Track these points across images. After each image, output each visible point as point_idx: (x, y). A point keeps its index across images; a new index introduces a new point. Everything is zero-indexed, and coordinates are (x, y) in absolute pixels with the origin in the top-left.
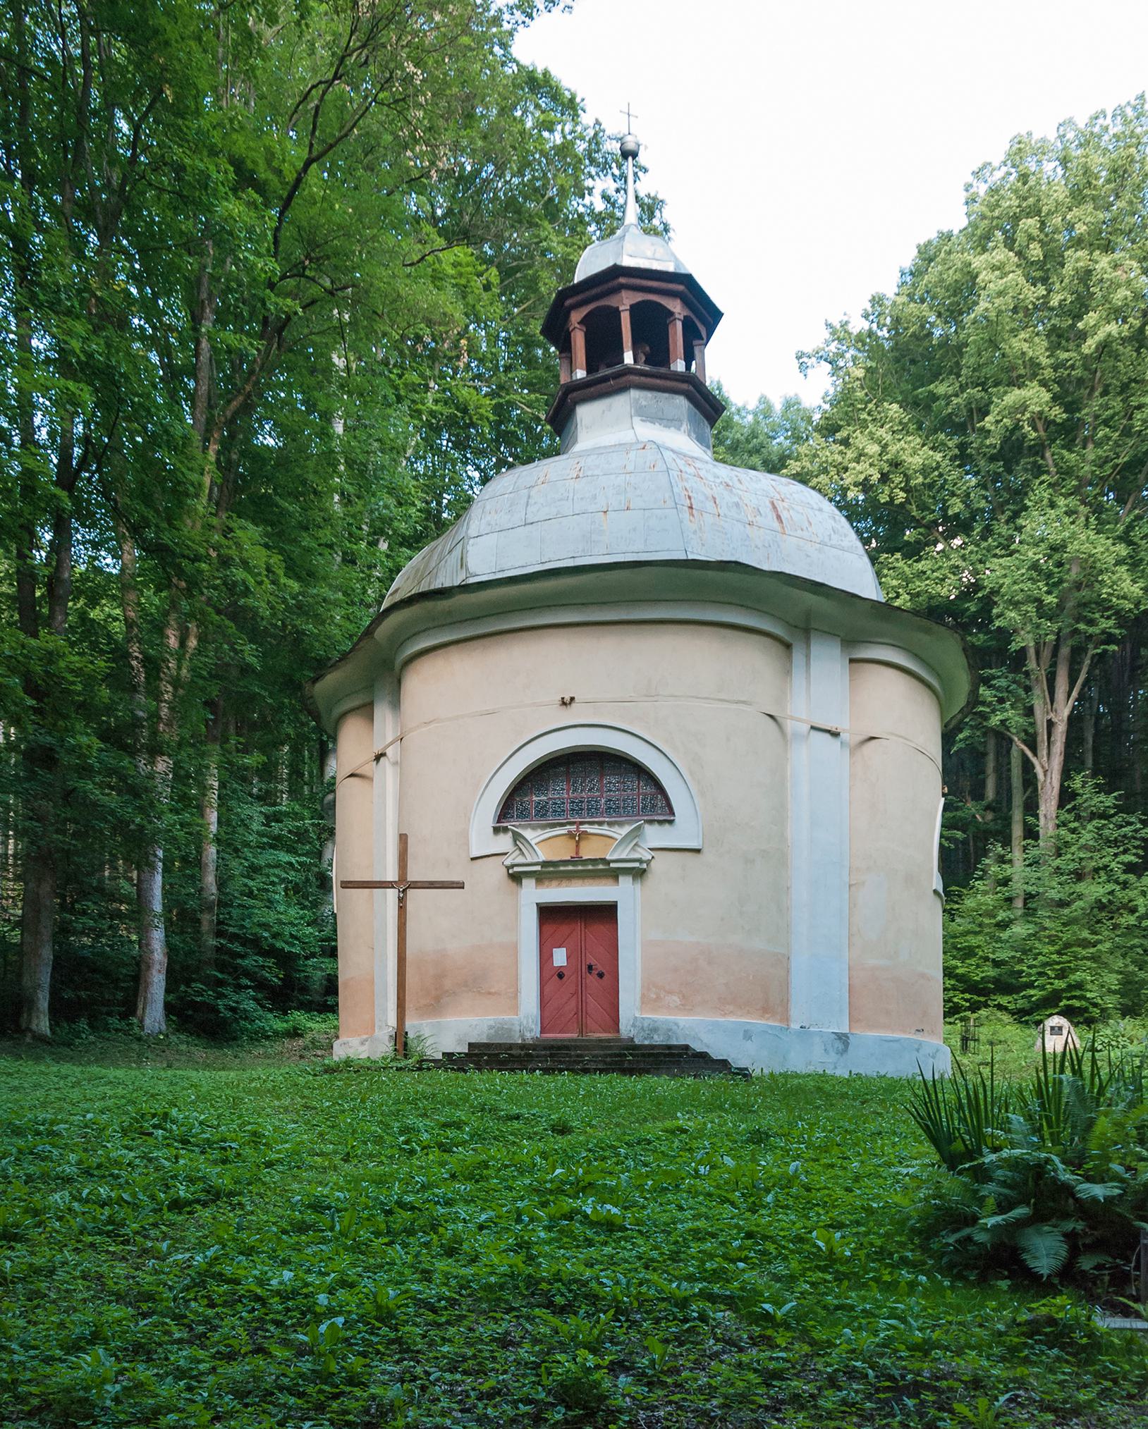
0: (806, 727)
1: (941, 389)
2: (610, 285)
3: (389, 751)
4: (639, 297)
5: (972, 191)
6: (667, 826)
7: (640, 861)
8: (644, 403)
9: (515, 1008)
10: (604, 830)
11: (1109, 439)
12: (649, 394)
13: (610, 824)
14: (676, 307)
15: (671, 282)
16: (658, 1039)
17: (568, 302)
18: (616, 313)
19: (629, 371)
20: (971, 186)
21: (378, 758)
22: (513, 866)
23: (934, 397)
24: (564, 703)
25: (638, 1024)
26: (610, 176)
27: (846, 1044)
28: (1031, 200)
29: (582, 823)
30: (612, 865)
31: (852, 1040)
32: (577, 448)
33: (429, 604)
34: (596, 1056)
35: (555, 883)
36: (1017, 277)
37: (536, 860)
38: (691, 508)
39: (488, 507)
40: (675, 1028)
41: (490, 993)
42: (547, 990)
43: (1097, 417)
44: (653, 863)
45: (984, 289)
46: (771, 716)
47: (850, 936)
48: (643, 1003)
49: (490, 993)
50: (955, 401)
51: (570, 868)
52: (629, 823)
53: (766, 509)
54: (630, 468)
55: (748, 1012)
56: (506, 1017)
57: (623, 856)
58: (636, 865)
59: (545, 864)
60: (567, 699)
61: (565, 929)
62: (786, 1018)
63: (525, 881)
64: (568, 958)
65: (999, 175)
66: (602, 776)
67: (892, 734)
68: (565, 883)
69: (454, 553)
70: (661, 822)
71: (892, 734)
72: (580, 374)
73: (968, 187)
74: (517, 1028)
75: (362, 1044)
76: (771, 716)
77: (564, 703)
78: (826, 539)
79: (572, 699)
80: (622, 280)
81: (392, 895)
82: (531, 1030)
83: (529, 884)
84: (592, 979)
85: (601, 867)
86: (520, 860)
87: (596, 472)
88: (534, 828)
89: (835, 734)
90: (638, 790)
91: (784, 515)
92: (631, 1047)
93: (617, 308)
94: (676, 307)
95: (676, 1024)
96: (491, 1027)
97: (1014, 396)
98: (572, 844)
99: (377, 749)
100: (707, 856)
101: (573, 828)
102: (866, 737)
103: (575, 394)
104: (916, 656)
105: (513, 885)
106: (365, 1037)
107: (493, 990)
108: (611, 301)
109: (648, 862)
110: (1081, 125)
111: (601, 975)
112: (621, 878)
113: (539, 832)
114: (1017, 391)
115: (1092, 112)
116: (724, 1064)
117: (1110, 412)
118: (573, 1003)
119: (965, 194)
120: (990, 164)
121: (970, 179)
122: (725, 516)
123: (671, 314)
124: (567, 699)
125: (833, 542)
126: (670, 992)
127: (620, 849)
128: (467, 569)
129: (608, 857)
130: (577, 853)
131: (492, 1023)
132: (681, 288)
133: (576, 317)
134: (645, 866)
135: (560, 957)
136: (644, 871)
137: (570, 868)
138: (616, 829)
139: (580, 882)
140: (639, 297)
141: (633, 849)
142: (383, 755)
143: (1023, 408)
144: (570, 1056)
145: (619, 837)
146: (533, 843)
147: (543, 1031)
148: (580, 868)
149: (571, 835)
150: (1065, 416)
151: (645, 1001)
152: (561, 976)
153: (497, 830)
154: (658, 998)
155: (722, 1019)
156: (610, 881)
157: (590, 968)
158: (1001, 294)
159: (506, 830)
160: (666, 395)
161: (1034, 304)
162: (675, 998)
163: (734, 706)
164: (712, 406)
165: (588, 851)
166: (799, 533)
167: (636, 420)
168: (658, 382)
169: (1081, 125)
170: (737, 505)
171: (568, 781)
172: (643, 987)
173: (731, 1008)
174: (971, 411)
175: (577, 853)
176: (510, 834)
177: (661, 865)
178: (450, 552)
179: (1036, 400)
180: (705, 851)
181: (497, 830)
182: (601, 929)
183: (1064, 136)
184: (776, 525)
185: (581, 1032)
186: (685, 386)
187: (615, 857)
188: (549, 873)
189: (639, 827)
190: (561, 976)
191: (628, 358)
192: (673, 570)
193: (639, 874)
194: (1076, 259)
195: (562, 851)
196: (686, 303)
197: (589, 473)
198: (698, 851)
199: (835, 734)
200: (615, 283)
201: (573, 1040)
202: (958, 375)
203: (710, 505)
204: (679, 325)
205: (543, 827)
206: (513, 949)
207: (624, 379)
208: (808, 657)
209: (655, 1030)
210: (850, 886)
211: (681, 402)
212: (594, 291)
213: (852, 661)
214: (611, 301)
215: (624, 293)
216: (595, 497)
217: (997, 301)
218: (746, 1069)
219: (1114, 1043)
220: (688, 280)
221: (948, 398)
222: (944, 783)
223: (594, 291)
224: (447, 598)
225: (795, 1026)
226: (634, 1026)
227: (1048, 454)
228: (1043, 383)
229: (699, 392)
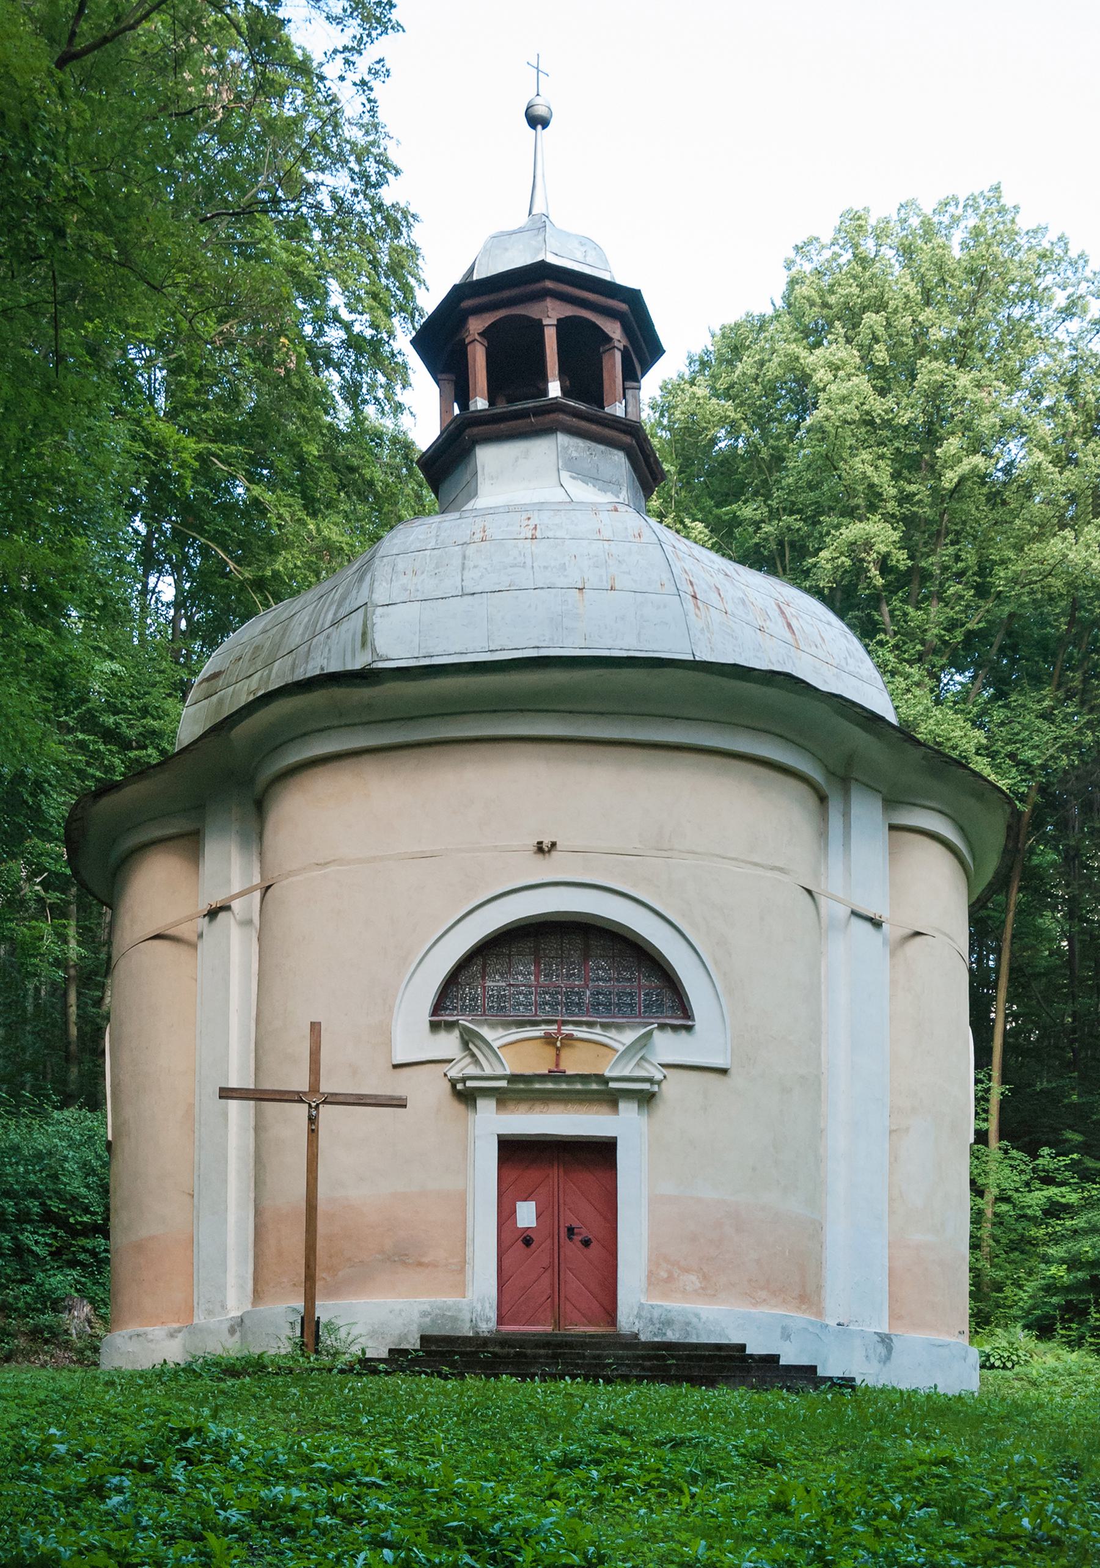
0: (843, 912)
1: (747, 511)
2: (538, 286)
3: (236, 905)
4: (569, 311)
5: (794, 270)
6: (683, 1034)
7: (650, 1080)
8: (574, 454)
9: (460, 1288)
10: (596, 1034)
11: (961, 597)
12: (580, 443)
13: (605, 1026)
14: (614, 330)
15: (612, 297)
16: (672, 1336)
17: (467, 304)
18: (538, 327)
19: (555, 407)
20: (793, 262)
21: (213, 914)
22: (464, 1080)
23: (736, 521)
24: (540, 849)
25: (644, 1313)
26: (346, 172)
27: (890, 1349)
28: (874, 291)
30: (612, 1085)
31: (896, 1343)
32: (482, 501)
33: (339, 693)
34: (622, 1358)
35: (523, 1107)
36: (862, 383)
37: (499, 1072)
38: (694, 597)
39: (400, 566)
40: (694, 1320)
43: (945, 568)
44: (664, 1085)
45: (824, 389)
46: (809, 892)
47: (891, 1200)
48: (649, 1284)
49: (420, 1264)
50: (766, 528)
51: (550, 1086)
52: (632, 1026)
53: (774, 613)
54: (607, 534)
55: (784, 1301)
56: (450, 1300)
57: (626, 1073)
58: (646, 1086)
59: (513, 1078)
60: (547, 842)
61: (533, 1175)
62: (820, 1313)
63: (481, 1103)
65: (827, 254)
66: (586, 957)
67: (938, 930)
68: (538, 1107)
69: (345, 626)
70: (675, 1028)
71: (938, 930)
72: (480, 403)
73: (789, 265)
74: (467, 1317)
75: (172, 1335)
76: (809, 892)
77: (540, 849)
78: (843, 663)
79: (554, 844)
80: (549, 284)
81: (300, 1111)
82: (488, 1320)
83: (486, 1107)
84: (572, 1249)
85: (594, 1086)
86: (472, 1070)
87: (559, 534)
88: (493, 1026)
89: (876, 924)
90: (645, 984)
91: (794, 623)
92: (631, 1343)
93: (540, 321)
94: (614, 330)
95: (697, 1316)
96: (425, 1314)
97: (853, 531)
99: (216, 900)
100: (736, 1079)
101: (553, 1028)
102: (909, 931)
103: (475, 430)
104: (962, 829)
105: (459, 1108)
106: (176, 1326)
107: (425, 1260)
108: (532, 311)
109: (659, 1083)
110: (928, 210)
111: (586, 1243)
112: (622, 1105)
113: (501, 1032)
114: (859, 525)
115: (942, 197)
116: (807, 1373)
117: (961, 565)
118: (546, 1280)
119: (785, 273)
120: (817, 239)
121: (792, 254)
122: (733, 615)
123: (608, 339)
124: (547, 842)
125: (851, 668)
126: (687, 1270)
127: (624, 1062)
128: (374, 650)
130: (557, 1065)
131: (427, 1307)
132: (624, 307)
133: (476, 326)
134: (656, 1088)
135: (526, 1215)
136: (653, 1095)
137: (550, 1086)
138: (613, 1033)
139: (561, 1107)
140: (569, 311)
141: (638, 1064)
142: (226, 908)
143: (868, 546)
144: (584, 1357)
145: (621, 1048)
146: (495, 1045)
147: (500, 1320)
148: (564, 1086)
149: (549, 1039)
150: (910, 563)
151: (653, 1280)
152: (528, 1242)
153: (435, 1026)
154: (670, 1279)
155: (753, 1311)
156: (605, 1109)
157: (571, 1231)
158: (844, 400)
159: (450, 1026)
160: (602, 447)
161: (882, 419)
162: (693, 1278)
163: (769, 874)
164: (652, 472)
165: (574, 1063)
166: (813, 650)
167: (565, 475)
168: (594, 427)
169: (928, 210)
170: (743, 602)
171: (537, 964)
172: (649, 1260)
173: (763, 1294)
174: (781, 543)
175: (557, 1065)
176: (456, 1033)
177: (674, 1087)
178: (335, 623)
179: (882, 538)
180: (733, 1071)
181: (435, 1026)
182: (589, 1179)
183: (905, 221)
184: (788, 635)
185: (557, 1324)
186: (627, 439)
188: (578, 1092)
190: (528, 1242)
191: (554, 389)
192: (690, 675)
193: (646, 1099)
194: (931, 370)
195: (536, 1062)
196: (627, 330)
197: (550, 534)
198: (724, 1071)
199: (876, 924)
200: (538, 286)
201: (547, 1335)
202: (768, 496)
203: (713, 598)
204: (618, 355)
205: (507, 1025)
206: (460, 1202)
207: (552, 416)
208: (846, 815)
209: (668, 1323)
210: (892, 1132)
211: (619, 458)
212: (506, 294)
213: (893, 828)
214: (532, 311)
215: (549, 303)
216: (563, 567)
217: (842, 409)
218: (853, 1379)
219: (1014, 1358)
220: (633, 297)
221: (757, 525)
223: (506, 294)
224: (369, 685)
225: (832, 1322)
226: (639, 1316)
227: (886, 609)
228: (888, 518)
229: (642, 451)
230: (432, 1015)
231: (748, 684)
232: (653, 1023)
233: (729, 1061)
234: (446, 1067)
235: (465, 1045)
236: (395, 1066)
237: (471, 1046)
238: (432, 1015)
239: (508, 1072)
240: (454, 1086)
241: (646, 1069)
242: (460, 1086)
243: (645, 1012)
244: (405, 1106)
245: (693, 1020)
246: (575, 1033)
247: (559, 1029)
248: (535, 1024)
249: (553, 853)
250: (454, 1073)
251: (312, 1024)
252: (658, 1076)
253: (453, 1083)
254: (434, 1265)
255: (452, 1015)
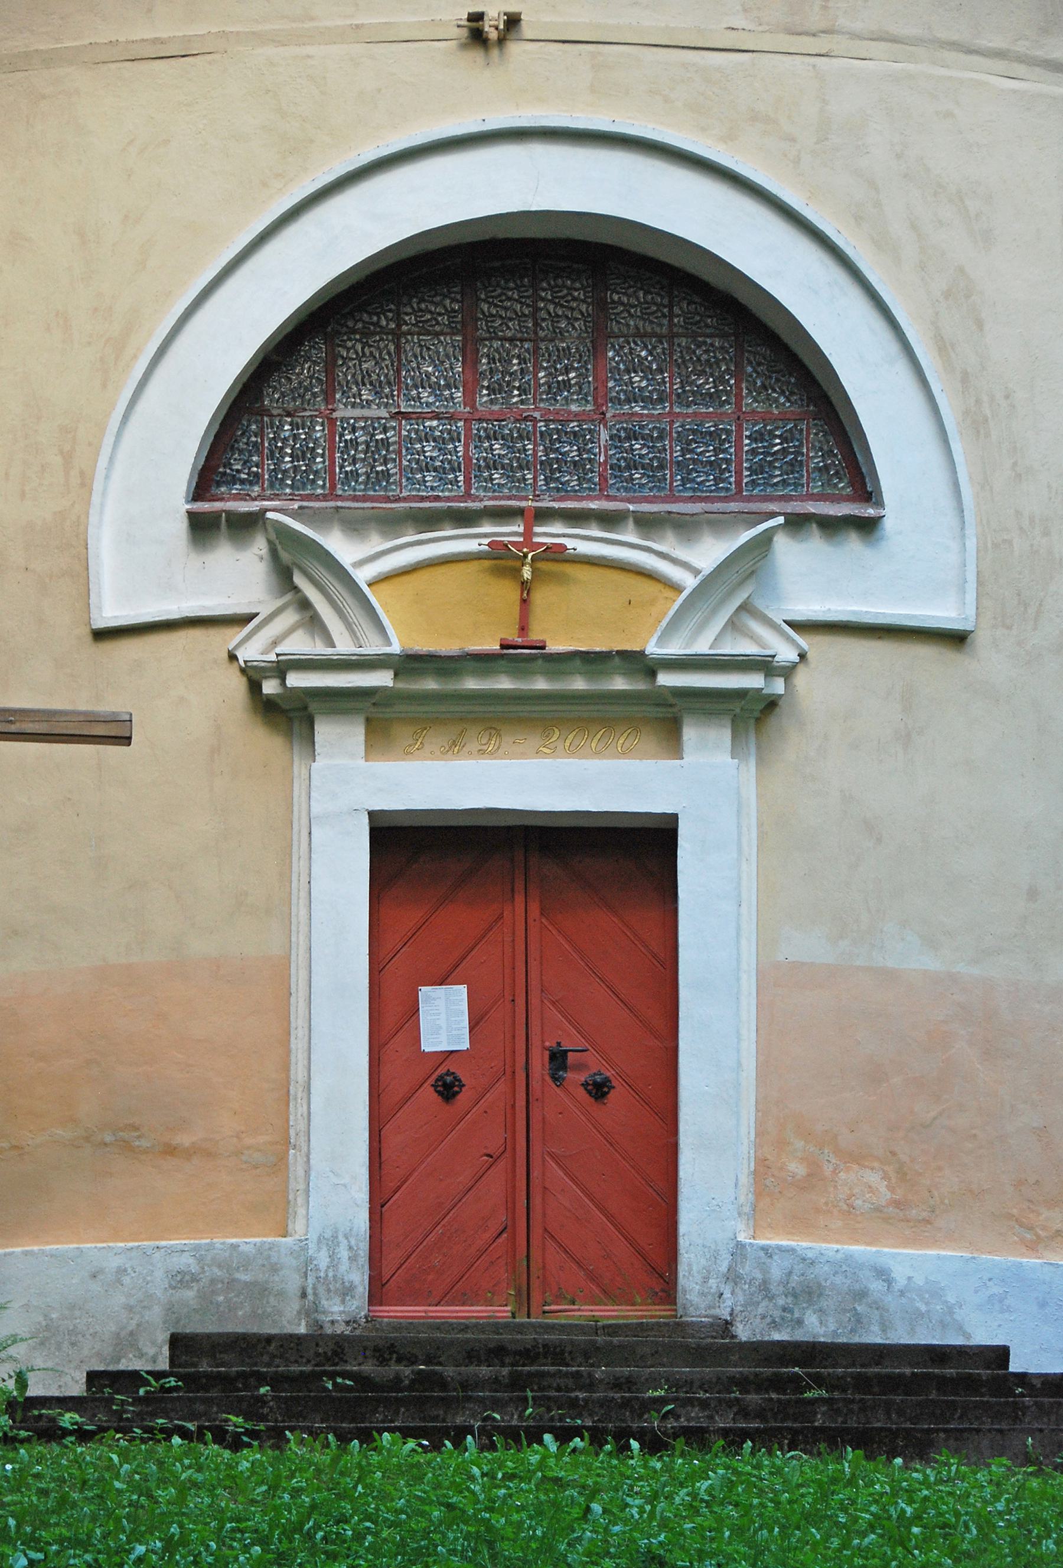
6: (853, 544)
7: (765, 665)
13: (647, 524)
22: (281, 669)
25: (747, 1269)
29: (543, 516)
30: (665, 679)
35: (436, 740)
37: (373, 647)
40: (876, 1286)
41: (170, 1150)
42: (393, 1140)
44: (801, 679)
48: (759, 1194)
49: (170, 1150)
51: (504, 683)
52: (720, 524)
56: (248, 1243)
57: (702, 647)
58: (753, 681)
63: (325, 731)
64: (475, 1024)
70: (830, 526)
74: (292, 1283)
79: (513, 21)
82: (346, 1291)
85: (620, 684)
86: (300, 645)
95: (883, 1274)
96: (181, 1279)
98: (508, 593)
101: (511, 531)
107: (184, 1140)
109: (788, 672)
111: (599, 1090)
112: (690, 733)
113: (376, 543)
118: (495, 1183)
126: (857, 1158)
129: (653, 649)
130: (523, 629)
131: (186, 1261)
134: (778, 686)
136: (771, 704)
137: (504, 683)
139: (534, 741)
141: (733, 625)
144: (591, 1385)
145: (690, 582)
146: (362, 576)
147: (377, 1292)
148: (541, 684)
152: (448, 1089)
154: (813, 1179)
156: (647, 741)
157: (558, 1059)
171: (471, 359)
172: (761, 1133)
175: (523, 629)
176: (260, 546)
180: (982, 639)
185: (525, 1298)
187: (674, 649)
189: (764, 542)
198: (957, 639)
222: (367, 277)
226: (732, 1277)
236: (102, 635)
237: (299, 580)
242: (270, 687)
248: (464, 519)
249: (514, 48)
250: (252, 652)
253: (253, 677)
254: (204, 1152)
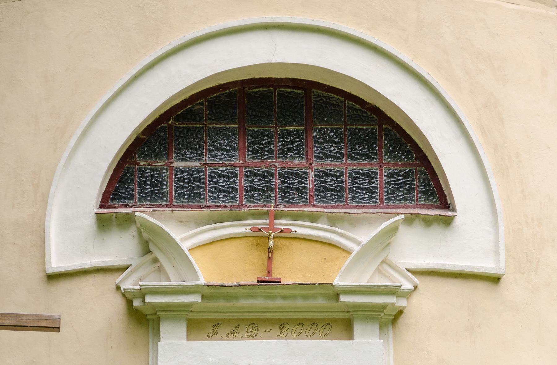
6: (436, 230)
7: (394, 291)
13: (333, 221)
22: (142, 293)
44: (416, 299)
52: (370, 222)
70: (428, 222)
109: (407, 295)
134: (402, 303)
141: (378, 270)
145: (356, 248)
198: (495, 280)
230: (102, 206)
231: (194, 232)
232: (398, 214)
233: (502, 264)
234: (119, 278)
235: (146, 249)
238: (102, 206)
239: (202, 281)
240: (129, 303)
241: (388, 278)
243: (389, 199)
244: (57, 329)
245: (454, 210)
246: (293, 229)
247: (271, 224)
251: (59, 328)
252: (407, 286)
255: (128, 206)
